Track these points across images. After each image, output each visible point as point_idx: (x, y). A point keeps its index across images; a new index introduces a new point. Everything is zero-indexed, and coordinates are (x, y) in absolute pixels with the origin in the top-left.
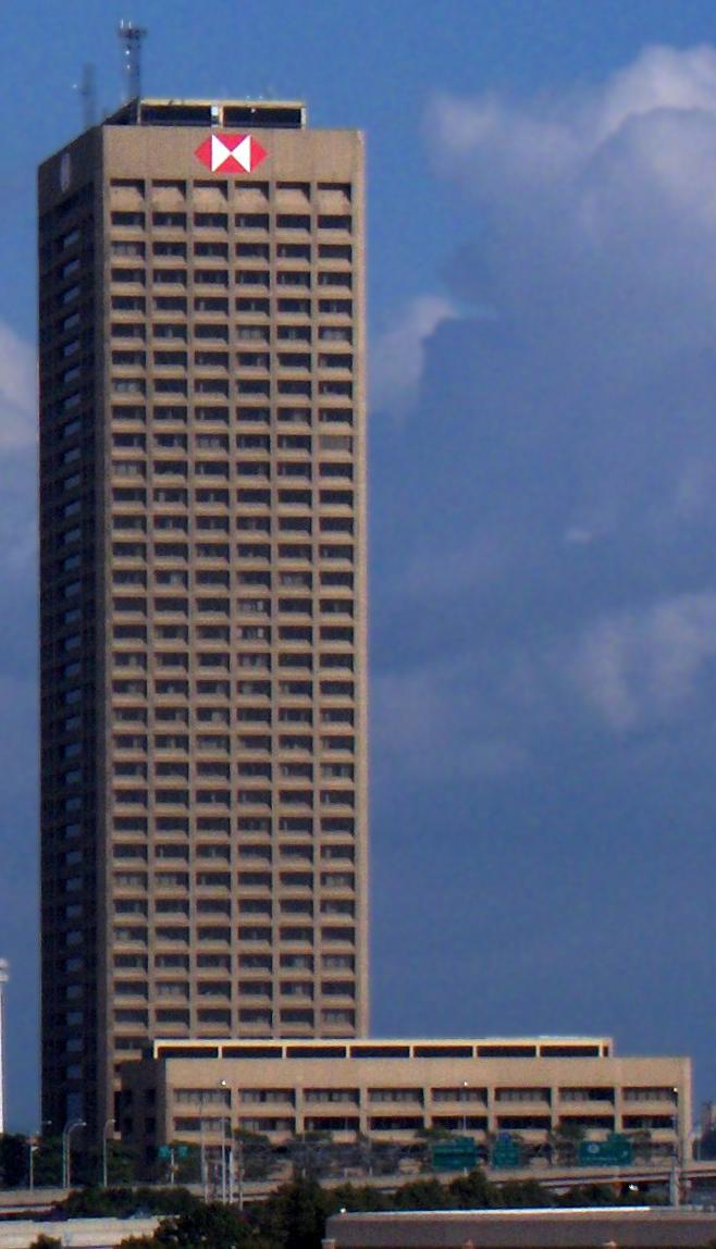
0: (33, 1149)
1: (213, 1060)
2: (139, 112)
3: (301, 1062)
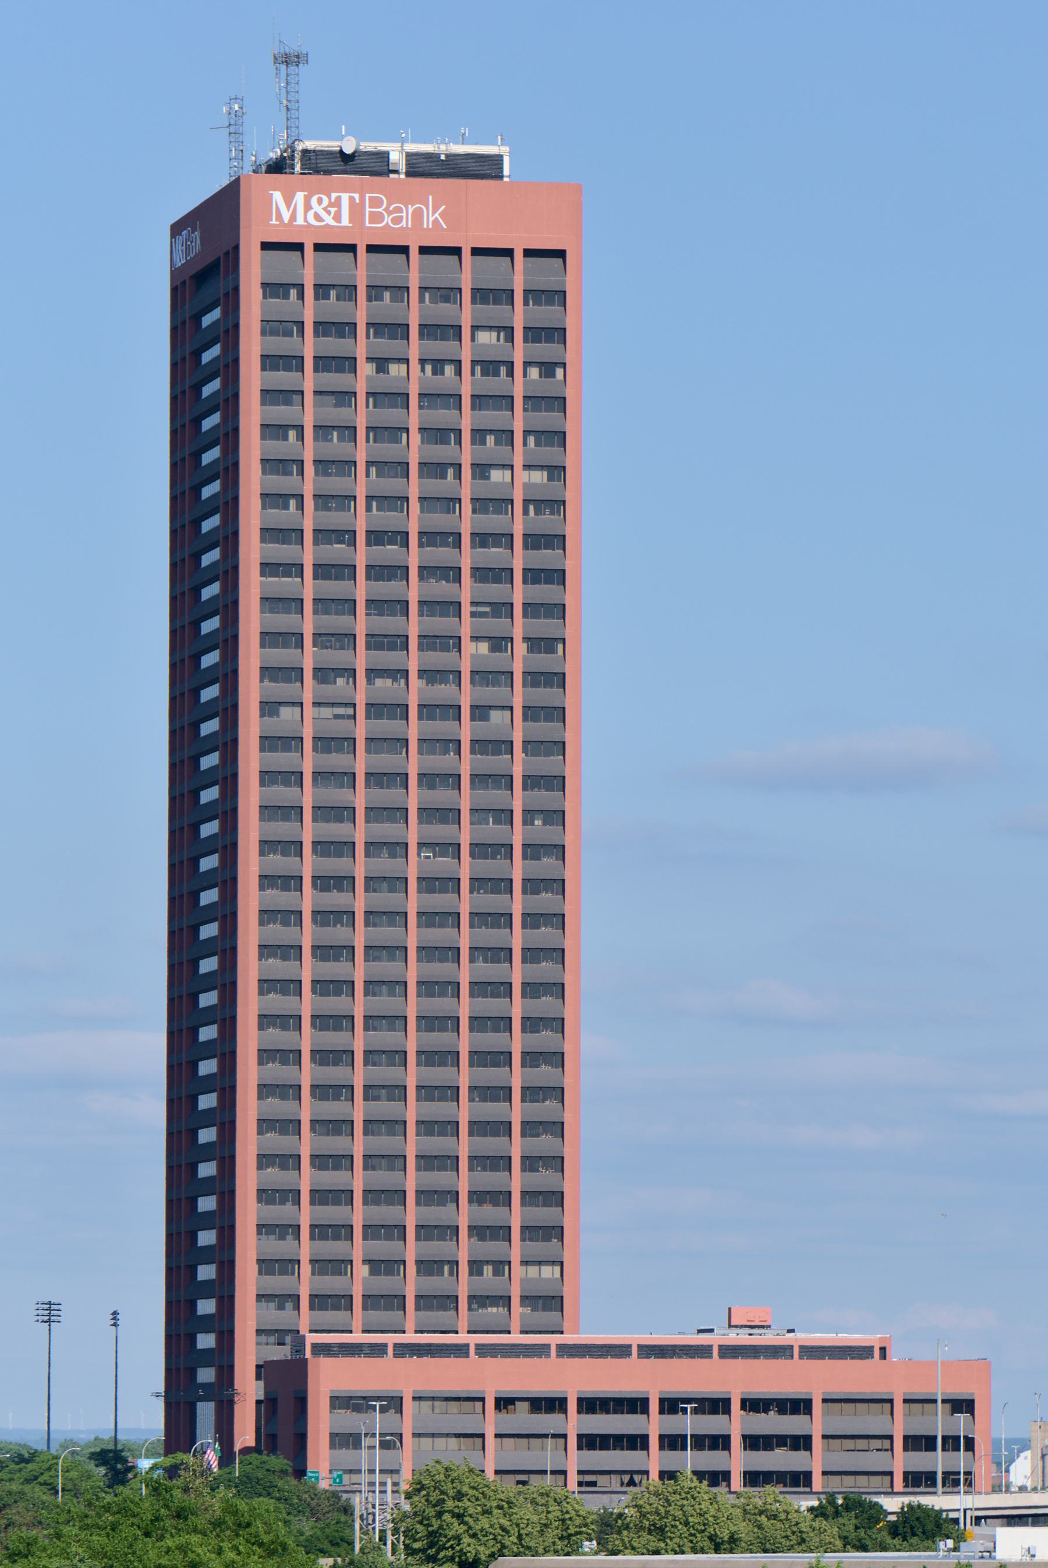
0: (145, 1464)
1: (543, 1360)
2: (298, 157)
3: (740, 1363)
